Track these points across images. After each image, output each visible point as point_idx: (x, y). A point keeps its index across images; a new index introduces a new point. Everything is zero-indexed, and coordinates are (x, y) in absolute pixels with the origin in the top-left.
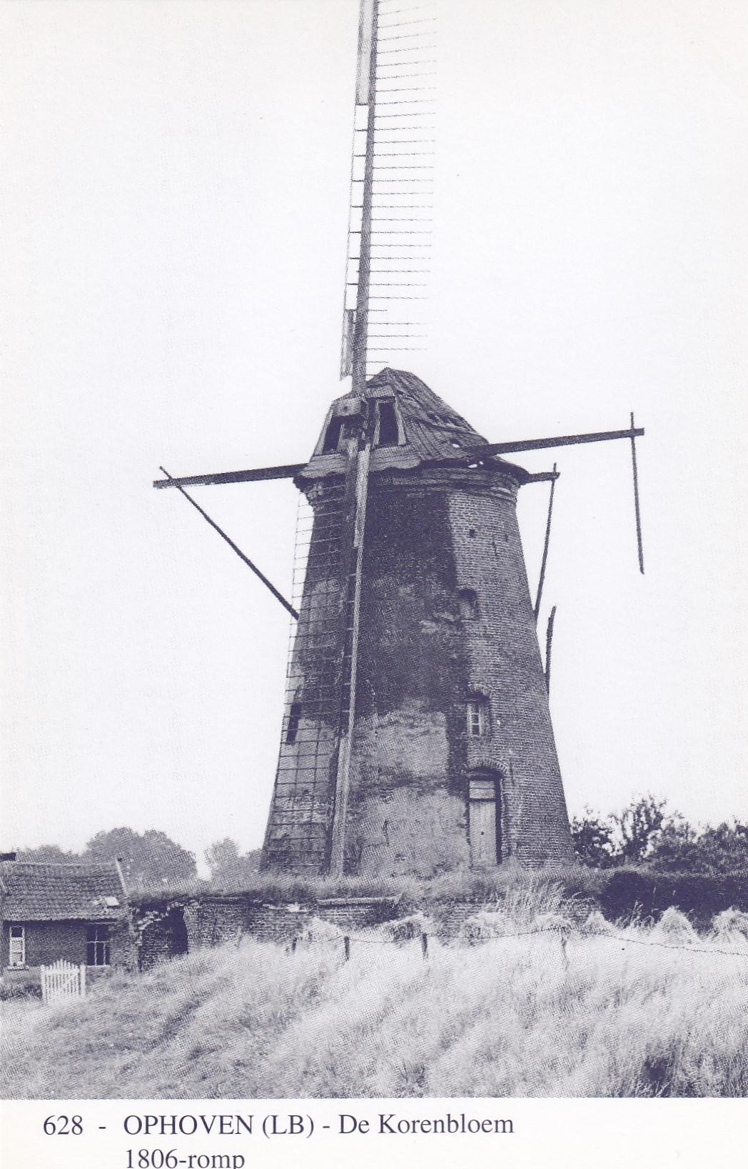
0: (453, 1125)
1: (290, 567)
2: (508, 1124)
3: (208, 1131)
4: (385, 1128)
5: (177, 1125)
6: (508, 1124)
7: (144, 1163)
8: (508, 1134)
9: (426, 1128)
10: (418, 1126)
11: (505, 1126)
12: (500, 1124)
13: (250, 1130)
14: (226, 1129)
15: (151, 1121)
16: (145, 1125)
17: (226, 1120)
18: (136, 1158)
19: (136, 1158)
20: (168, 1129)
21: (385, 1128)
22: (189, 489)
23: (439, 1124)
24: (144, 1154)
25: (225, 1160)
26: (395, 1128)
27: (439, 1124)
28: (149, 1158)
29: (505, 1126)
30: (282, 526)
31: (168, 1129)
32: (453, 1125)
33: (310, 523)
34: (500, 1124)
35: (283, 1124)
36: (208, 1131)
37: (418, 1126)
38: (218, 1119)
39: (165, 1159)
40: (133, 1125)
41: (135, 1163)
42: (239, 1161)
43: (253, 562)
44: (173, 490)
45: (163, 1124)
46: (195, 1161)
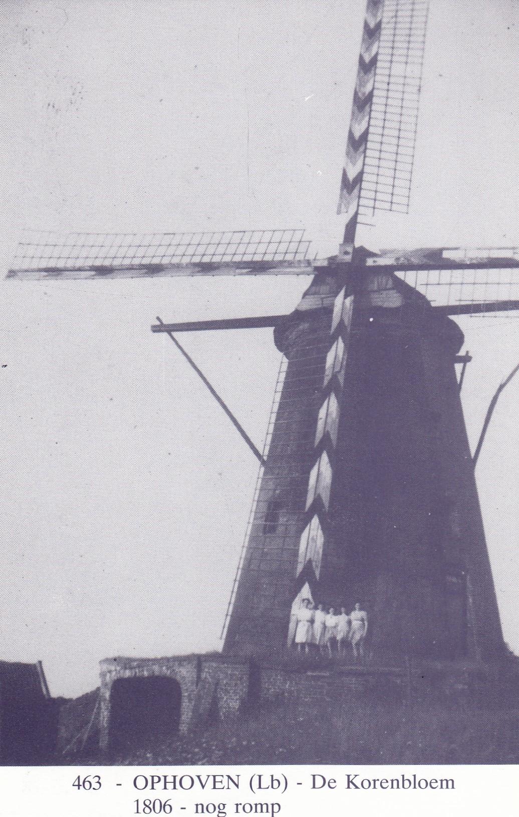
0: (407, 783)
1: (261, 415)
2: (450, 783)
3: (203, 787)
4: (351, 785)
5: (177, 783)
6: (450, 783)
7: (147, 810)
8: (450, 790)
9: (384, 785)
10: (378, 783)
11: (448, 784)
12: (444, 783)
13: (237, 786)
14: (218, 785)
15: (156, 779)
16: (151, 782)
17: (218, 779)
18: (141, 806)
19: (141, 806)
20: (170, 786)
21: (351, 785)
22: (182, 337)
23: (395, 783)
24: (147, 803)
25: (265, 807)
26: (359, 785)
27: (395, 783)
28: (151, 806)
29: (448, 784)
30: (257, 372)
31: (170, 786)
32: (407, 783)
33: (285, 367)
34: (444, 783)
35: (266, 782)
36: (203, 787)
37: (378, 783)
38: (211, 778)
39: (163, 807)
40: (141, 782)
41: (141, 810)
42: (276, 807)
43: (229, 407)
44: (165, 335)
45: (165, 782)
46: (240, 807)
